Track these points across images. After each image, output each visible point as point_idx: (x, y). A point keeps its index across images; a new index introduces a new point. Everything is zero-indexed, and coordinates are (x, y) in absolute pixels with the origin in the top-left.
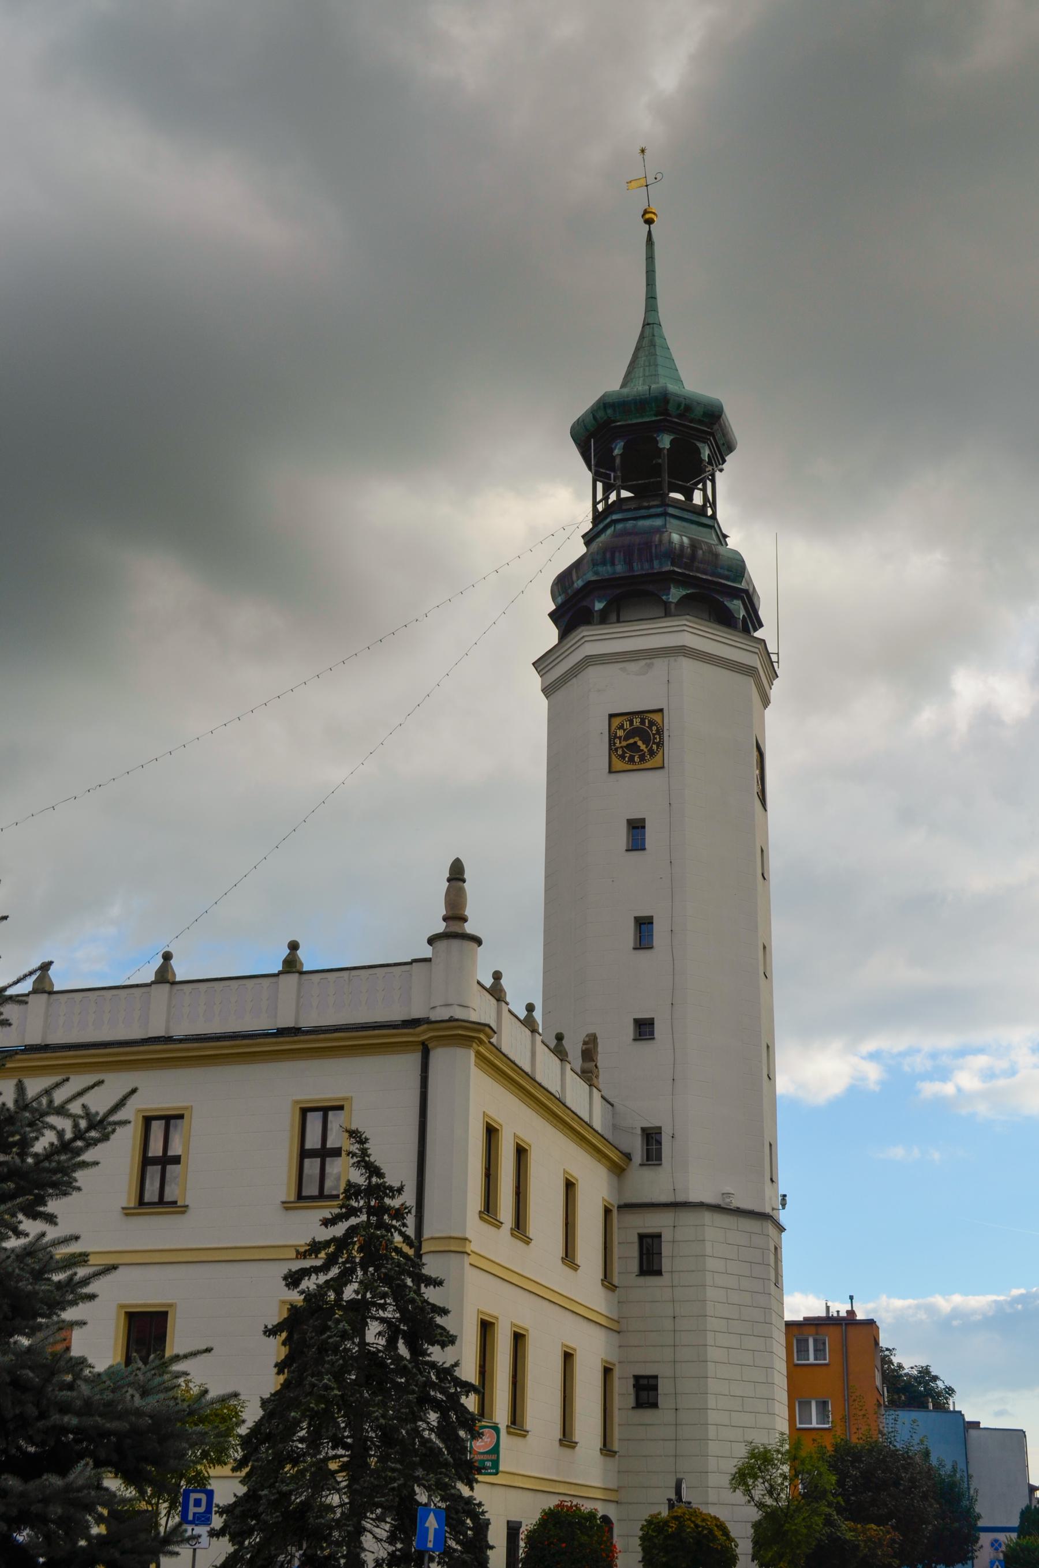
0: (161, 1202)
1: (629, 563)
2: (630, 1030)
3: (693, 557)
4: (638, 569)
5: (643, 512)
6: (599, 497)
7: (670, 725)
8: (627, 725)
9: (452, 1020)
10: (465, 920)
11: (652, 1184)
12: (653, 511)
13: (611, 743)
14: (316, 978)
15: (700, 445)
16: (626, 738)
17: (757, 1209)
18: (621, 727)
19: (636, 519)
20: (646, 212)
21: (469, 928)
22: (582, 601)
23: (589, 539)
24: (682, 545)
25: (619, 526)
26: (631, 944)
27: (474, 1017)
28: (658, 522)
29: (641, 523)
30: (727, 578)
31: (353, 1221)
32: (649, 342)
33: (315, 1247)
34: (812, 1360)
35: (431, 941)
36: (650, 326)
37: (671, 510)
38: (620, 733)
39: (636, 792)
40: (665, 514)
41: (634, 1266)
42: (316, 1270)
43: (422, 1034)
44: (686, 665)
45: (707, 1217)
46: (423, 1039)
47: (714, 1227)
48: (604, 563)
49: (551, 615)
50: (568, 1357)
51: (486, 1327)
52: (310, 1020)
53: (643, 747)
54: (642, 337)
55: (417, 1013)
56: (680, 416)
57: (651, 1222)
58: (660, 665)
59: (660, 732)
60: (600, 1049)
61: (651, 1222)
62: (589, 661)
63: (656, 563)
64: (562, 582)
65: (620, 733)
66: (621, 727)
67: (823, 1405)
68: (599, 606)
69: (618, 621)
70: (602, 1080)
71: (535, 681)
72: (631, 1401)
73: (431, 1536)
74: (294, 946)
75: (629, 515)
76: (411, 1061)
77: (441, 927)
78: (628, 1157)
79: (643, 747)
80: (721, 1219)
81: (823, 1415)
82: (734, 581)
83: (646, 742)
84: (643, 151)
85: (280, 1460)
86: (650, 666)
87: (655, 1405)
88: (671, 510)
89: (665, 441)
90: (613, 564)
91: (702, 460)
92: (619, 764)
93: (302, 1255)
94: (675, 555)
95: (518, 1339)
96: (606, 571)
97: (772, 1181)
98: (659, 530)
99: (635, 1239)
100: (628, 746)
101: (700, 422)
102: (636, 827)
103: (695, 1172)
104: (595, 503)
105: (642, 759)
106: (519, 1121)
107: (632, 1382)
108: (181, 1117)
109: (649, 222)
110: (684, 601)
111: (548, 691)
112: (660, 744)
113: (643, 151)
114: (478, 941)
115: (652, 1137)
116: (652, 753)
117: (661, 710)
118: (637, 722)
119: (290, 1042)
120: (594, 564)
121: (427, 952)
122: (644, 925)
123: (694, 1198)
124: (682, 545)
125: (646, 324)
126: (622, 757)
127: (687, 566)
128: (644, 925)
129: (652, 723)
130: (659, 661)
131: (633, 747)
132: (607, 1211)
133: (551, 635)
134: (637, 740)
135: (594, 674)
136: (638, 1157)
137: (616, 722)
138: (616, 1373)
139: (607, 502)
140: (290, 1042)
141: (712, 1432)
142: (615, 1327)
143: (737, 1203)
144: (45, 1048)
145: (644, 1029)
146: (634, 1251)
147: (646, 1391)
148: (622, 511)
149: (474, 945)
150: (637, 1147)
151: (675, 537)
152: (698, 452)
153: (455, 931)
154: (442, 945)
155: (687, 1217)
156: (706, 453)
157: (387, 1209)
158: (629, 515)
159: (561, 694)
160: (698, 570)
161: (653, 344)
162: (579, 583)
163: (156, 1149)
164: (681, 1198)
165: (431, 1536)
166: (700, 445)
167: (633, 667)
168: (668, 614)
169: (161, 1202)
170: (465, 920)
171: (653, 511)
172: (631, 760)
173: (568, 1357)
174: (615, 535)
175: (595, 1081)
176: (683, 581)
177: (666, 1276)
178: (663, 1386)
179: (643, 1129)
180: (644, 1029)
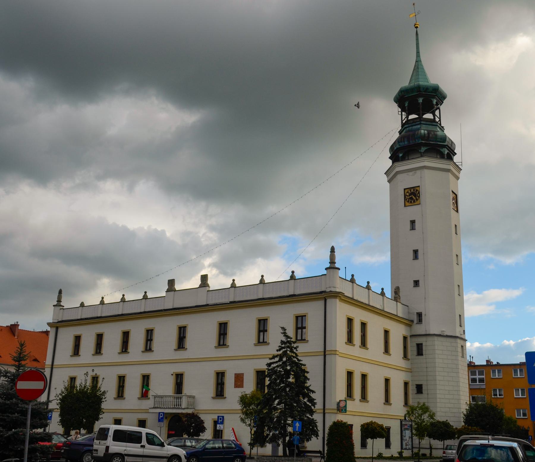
0: (264, 342)
1: (409, 141)
2: (412, 284)
3: (429, 136)
4: (412, 142)
5: (414, 124)
6: (404, 117)
7: (422, 191)
8: (409, 191)
9: (331, 291)
10: (335, 263)
11: (419, 329)
12: (417, 123)
13: (405, 197)
14: (298, 281)
15: (432, 99)
16: (409, 196)
17: (453, 335)
18: (408, 192)
19: (412, 126)
20: (415, 25)
21: (337, 265)
22: (401, 152)
23: (400, 132)
24: (425, 134)
25: (407, 129)
26: (412, 258)
27: (338, 290)
28: (419, 126)
29: (414, 127)
30: (440, 142)
31: (284, 350)
32: (418, 67)
33: (274, 357)
34: (519, 376)
35: (326, 269)
36: (418, 61)
37: (422, 122)
38: (408, 194)
39: (413, 212)
40: (421, 124)
41: (415, 353)
42: (276, 362)
43: (323, 295)
44: (426, 171)
45: (436, 338)
46: (325, 296)
47: (438, 341)
48: (401, 142)
49: (390, 158)
50: (387, 381)
51: (350, 374)
52: (298, 292)
53: (414, 198)
54: (415, 66)
55: (323, 290)
56: (425, 92)
57: (420, 340)
58: (418, 172)
59: (419, 193)
60: (400, 290)
61: (420, 340)
62: (398, 173)
63: (417, 140)
64: (392, 148)
65: (408, 194)
66: (408, 192)
67: (523, 390)
68: (401, 155)
69: (408, 159)
70: (403, 299)
71: (385, 178)
72: (415, 392)
73: (297, 428)
74: (293, 272)
75: (410, 125)
76: (322, 303)
77: (328, 265)
78: (412, 321)
79: (414, 198)
80: (440, 339)
81: (523, 394)
82: (443, 142)
83: (415, 196)
84: (414, 4)
85: (303, 411)
86: (415, 173)
87: (422, 393)
88: (422, 122)
89: (420, 100)
90: (404, 142)
91: (433, 104)
92: (407, 204)
93: (271, 359)
94: (423, 137)
95: (364, 377)
96: (402, 144)
97: (461, 326)
98: (419, 129)
99: (415, 345)
100: (410, 198)
101: (432, 92)
102: (413, 222)
103: (432, 324)
104: (402, 121)
105: (414, 202)
106: (359, 316)
107: (415, 386)
108: (305, 316)
109: (417, 27)
110: (426, 151)
111: (389, 181)
112: (419, 197)
113: (414, 4)
114: (339, 269)
115: (420, 315)
116: (417, 200)
117: (419, 186)
118: (412, 190)
119: (292, 298)
120: (399, 142)
121: (325, 272)
122: (416, 252)
123: (432, 333)
124: (425, 134)
125: (416, 61)
126: (408, 201)
127: (426, 140)
128: (416, 252)
129: (417, 190)
130: (424, 172)
131: (411, 198)
132: (405, 338)
133: (390, 162)
134: (412, 196)
135: (399, 177)
136: (415, 321)
137: (406, 191)
138: (410, 384)
139: (407, 118)
140: (292, 298)
141: (438, 400)
142: (410, 371)
143: (445, 334)
144: (263, 299)
145: (416, 283)
146: (415, 349)
147: (419, 389)
148: (408, 124)
149: (338, 270)
150: (415, 318)
151: (422, 131)
152: (432, 101)
153: (332, 267)
154: (328, 270)
155: (430, 339)
156: (435, 101)
157: (293, 347)
158: (410, 125)
159: (392, 182)
160: (431, 141)
161: (418, 68)
162: (395, 148)
163: (300, 325)
164: (428, 333)
165: (297, 428)
166: (432, 99)
167: (411, 173)
168: (422, 156)
169: (264, 342)
170: (335, 263)
171: (417, 123)
172: (411, 202)
173: (387, 381)
174: (406, 132)
175: (398, 300)
176: (425, 145)
177: (424, 356)
178: (424, 388)
179: (417, 313)
180: (416, 283)
